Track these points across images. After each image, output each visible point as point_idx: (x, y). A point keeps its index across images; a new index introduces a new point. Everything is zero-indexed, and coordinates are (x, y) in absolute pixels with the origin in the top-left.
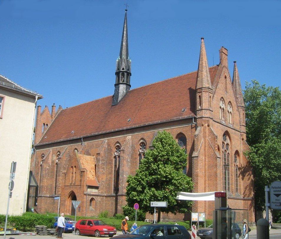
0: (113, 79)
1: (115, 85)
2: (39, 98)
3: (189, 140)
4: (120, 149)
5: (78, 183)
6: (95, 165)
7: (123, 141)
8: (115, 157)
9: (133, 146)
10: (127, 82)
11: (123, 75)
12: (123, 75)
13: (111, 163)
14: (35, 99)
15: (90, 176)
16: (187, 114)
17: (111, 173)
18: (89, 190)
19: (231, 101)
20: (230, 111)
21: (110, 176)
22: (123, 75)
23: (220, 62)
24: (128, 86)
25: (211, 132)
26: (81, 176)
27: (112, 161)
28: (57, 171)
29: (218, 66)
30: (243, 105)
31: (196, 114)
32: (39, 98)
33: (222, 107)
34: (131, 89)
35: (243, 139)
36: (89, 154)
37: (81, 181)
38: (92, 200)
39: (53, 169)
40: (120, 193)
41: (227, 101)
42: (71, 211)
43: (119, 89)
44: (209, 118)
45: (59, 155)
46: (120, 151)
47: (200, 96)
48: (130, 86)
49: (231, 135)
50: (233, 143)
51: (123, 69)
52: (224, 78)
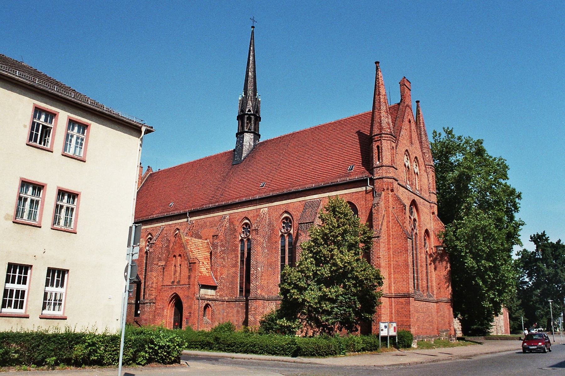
0: (235, 126)
1: (237, 134)
2: (147, 131)
3: (362, 213)
4: (249, 228)
5: (184, 281)
6: (211, 253)
7: (254, 217)
8: (242, 240)
9: (270, 224)
10: (255, 129)
11: (249, 119)
12: (249, 119)
13: (235, 250)
14: (141, 132)
15: (204, 269)
16: (358, 172)
17: (235, 266)
18: (203, 291)
19: (418, 157)
20: (416, 172)
21: (234, 269)
22: (249, 119)
23: (401, 100)
24: (257, 136)
25: (398, 199)
26: (189, 270)
27: (236, 246)
28: (146, 263)
29: (399, 104)
30: (432, 163)
31: (372, 174)
32: (147, 131)
33: (407, 164)
34: (261, 140)
35: (433, 213)
36: (200, 238)
37: (189, 277)
38: (207, 306)
39: (142, 261)
40: (252, 295)
41: (413, 157)
42: (172, 324)
43: (243, 140)
44: (394, 179)
45: (150, 239)
46: (249, 232)
47: (378, 147)
48: (259, 136)
49: (420, 206)
50: (422, 218)
51: (249, 111)
52: (407, 122)
